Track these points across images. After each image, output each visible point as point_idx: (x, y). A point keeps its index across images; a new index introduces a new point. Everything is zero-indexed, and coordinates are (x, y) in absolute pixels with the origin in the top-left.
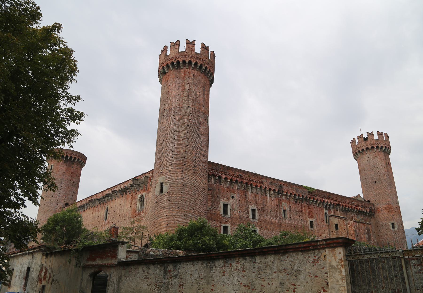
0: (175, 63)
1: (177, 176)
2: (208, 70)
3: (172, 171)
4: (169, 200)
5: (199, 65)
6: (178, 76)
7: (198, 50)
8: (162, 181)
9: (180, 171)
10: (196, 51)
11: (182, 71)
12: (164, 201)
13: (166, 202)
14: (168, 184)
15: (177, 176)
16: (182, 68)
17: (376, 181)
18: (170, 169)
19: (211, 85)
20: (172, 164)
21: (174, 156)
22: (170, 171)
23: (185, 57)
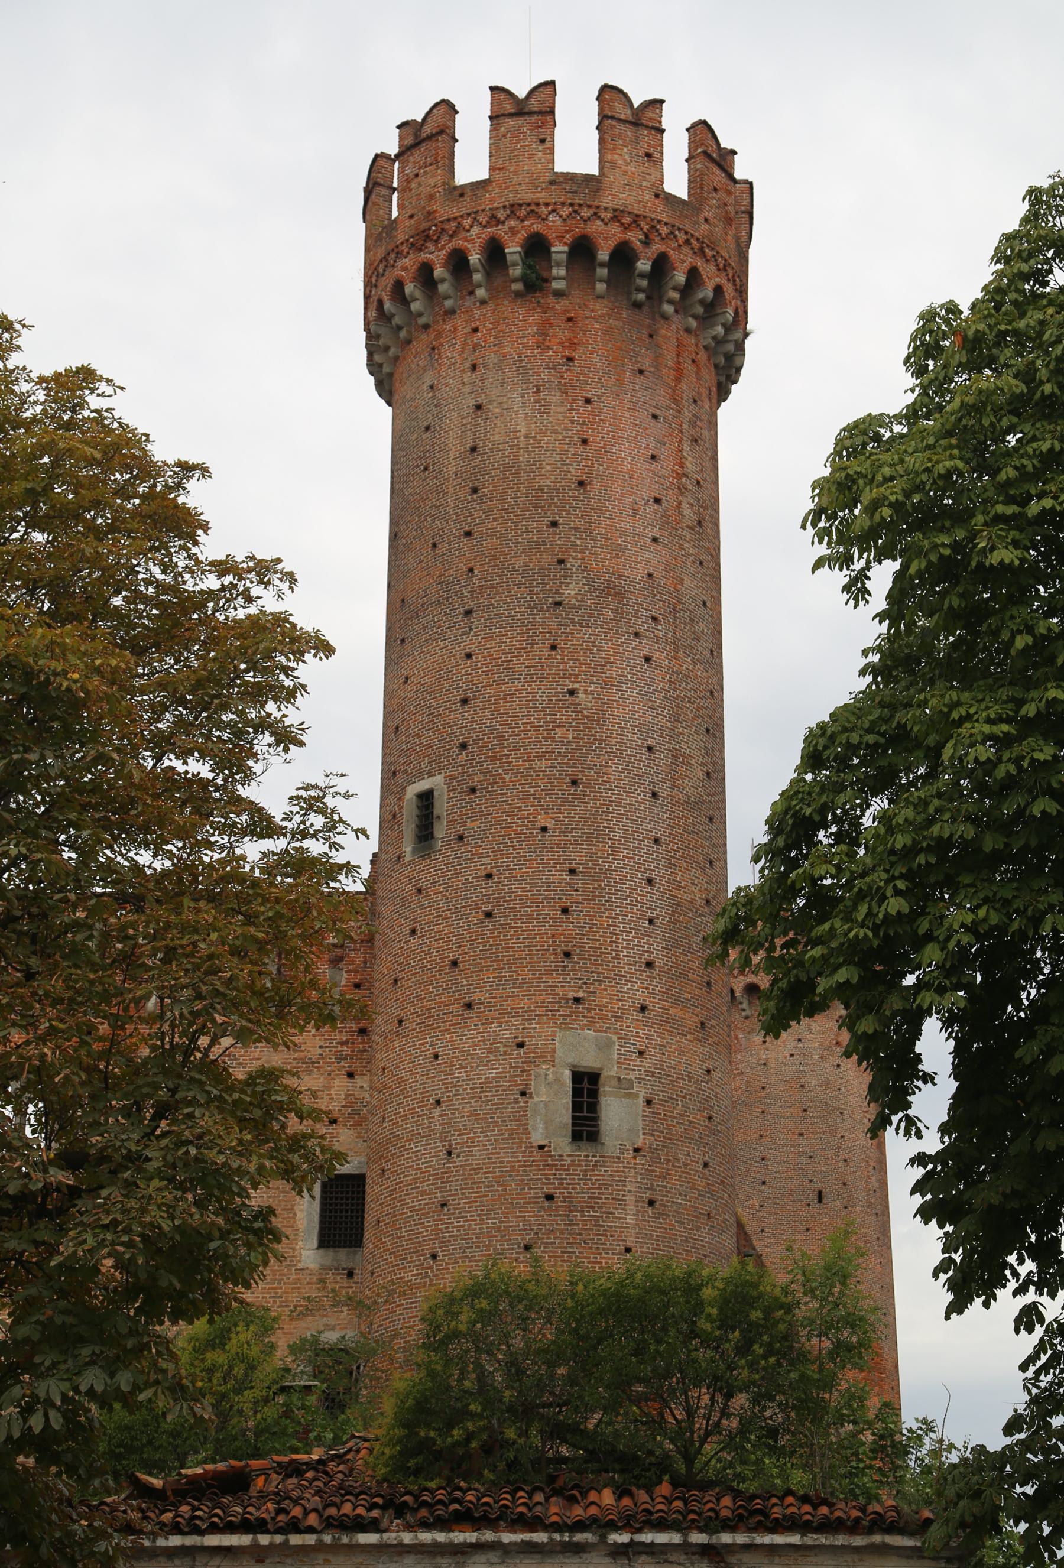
0: (438, 272)
1: (681, 1052)
2: (708, 293)
3: (655, 1006)
4: (651, 1203)
5: (513, 250)
6: (647, 364)
7: (576, 148)
8: (589, 1061)
9: (691, 1021)
10: (562, 165)
11: (670, 333)
12: (624, 1207)
13: (631, 1208)
14: (641, 1092)
15: (681, 1052)
16: (665, 317)
17: (826, 1190)
18: (641, 997)
19: (723, 394)
20: (649, 964)
21: (662, 915)
22: (643, 1009)
23: (494, 220)
